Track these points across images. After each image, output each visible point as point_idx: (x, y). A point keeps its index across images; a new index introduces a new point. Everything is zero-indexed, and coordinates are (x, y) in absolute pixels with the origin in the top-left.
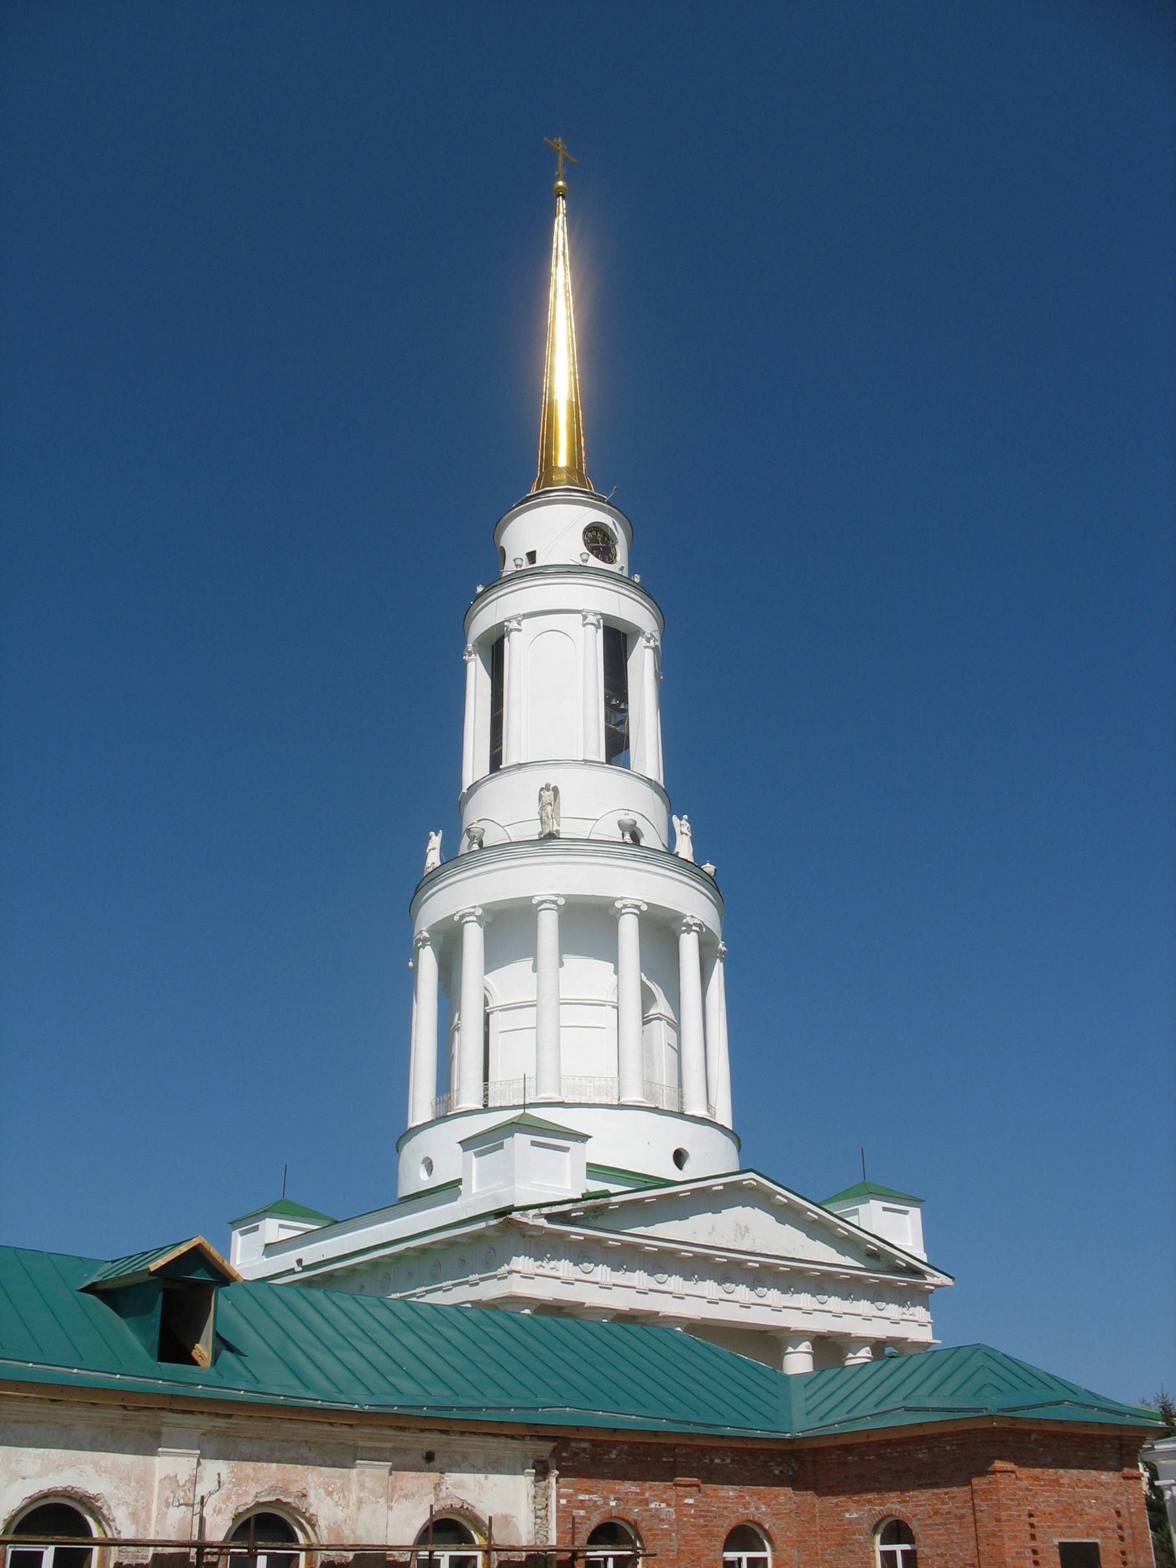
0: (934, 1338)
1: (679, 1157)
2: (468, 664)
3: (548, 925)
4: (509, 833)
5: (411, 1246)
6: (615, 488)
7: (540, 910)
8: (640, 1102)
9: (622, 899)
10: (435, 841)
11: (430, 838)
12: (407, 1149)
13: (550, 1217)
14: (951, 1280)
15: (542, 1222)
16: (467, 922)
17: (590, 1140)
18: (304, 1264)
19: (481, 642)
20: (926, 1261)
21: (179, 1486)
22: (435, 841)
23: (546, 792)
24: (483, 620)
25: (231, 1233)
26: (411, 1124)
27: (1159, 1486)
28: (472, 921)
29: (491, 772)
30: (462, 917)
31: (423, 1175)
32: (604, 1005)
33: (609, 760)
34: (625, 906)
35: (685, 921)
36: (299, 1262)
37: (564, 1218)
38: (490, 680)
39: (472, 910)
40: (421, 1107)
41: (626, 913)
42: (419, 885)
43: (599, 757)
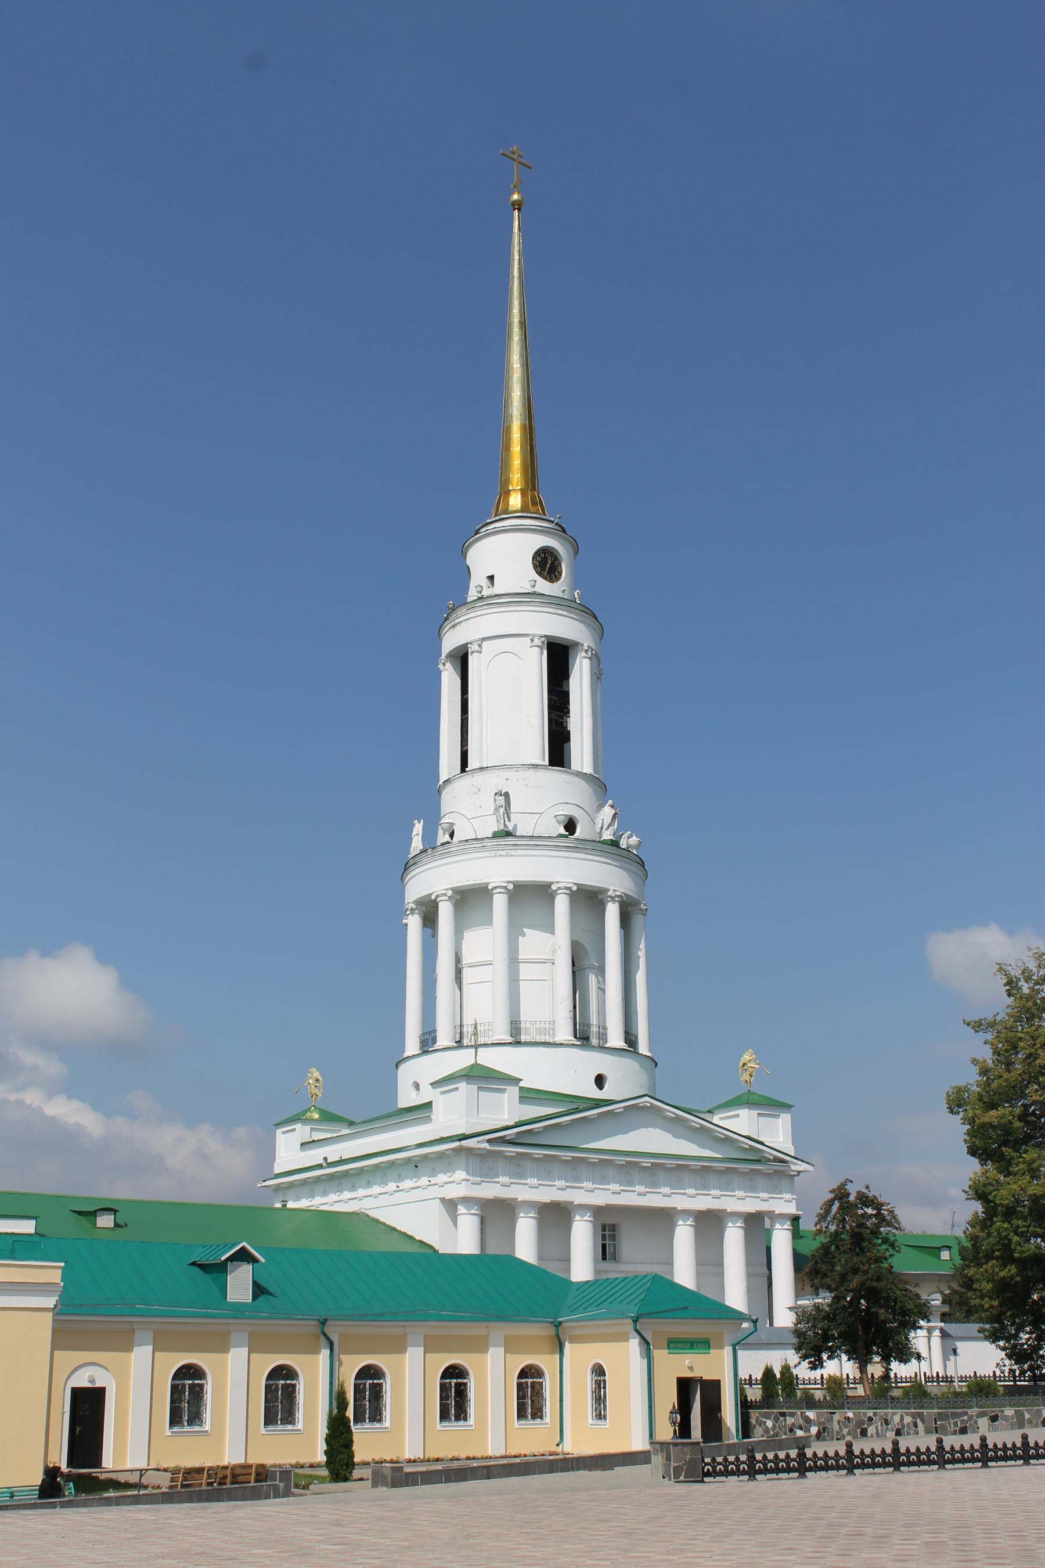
0: (797, 1211)
1: (600, 1081)
2: (442, 673)
3: (500, 902)
4: (474, 825)
5: (399, 1157)
6: (558, 516)
7: (495, 893)
8: (569, 1041)
9: (557, 882)
10: (418, 828)
11: (414, 825)
12: (403, 1067)
13: (489, 1141)
14: (811, 1167)
15: (487, 1146)
16: (441, 901)
17: (521, 1082)
18: (329, 1161)
19: (451, 656)
20: (793, 1155)
21: (323, 1323)
22: (418, 828)
23: (499, 797)
24: (451, 641)
25: (276, 1131)
26: (406, 1055)
27: (941, 1322)
28: (445, 900)
29: (462, 772)
30: (437, 896)
31: (413, 1093)
32: (546, 963)
33: (552, 763)
34: (559, 888)
35: (609, 894)
36: (325, 1159)
37: (503, 1141)
38: (460, 681)
39: (445, 892)
40: (412, 1046)
41: (560, 894)
42: (407, 863)
43: (544, 760)
